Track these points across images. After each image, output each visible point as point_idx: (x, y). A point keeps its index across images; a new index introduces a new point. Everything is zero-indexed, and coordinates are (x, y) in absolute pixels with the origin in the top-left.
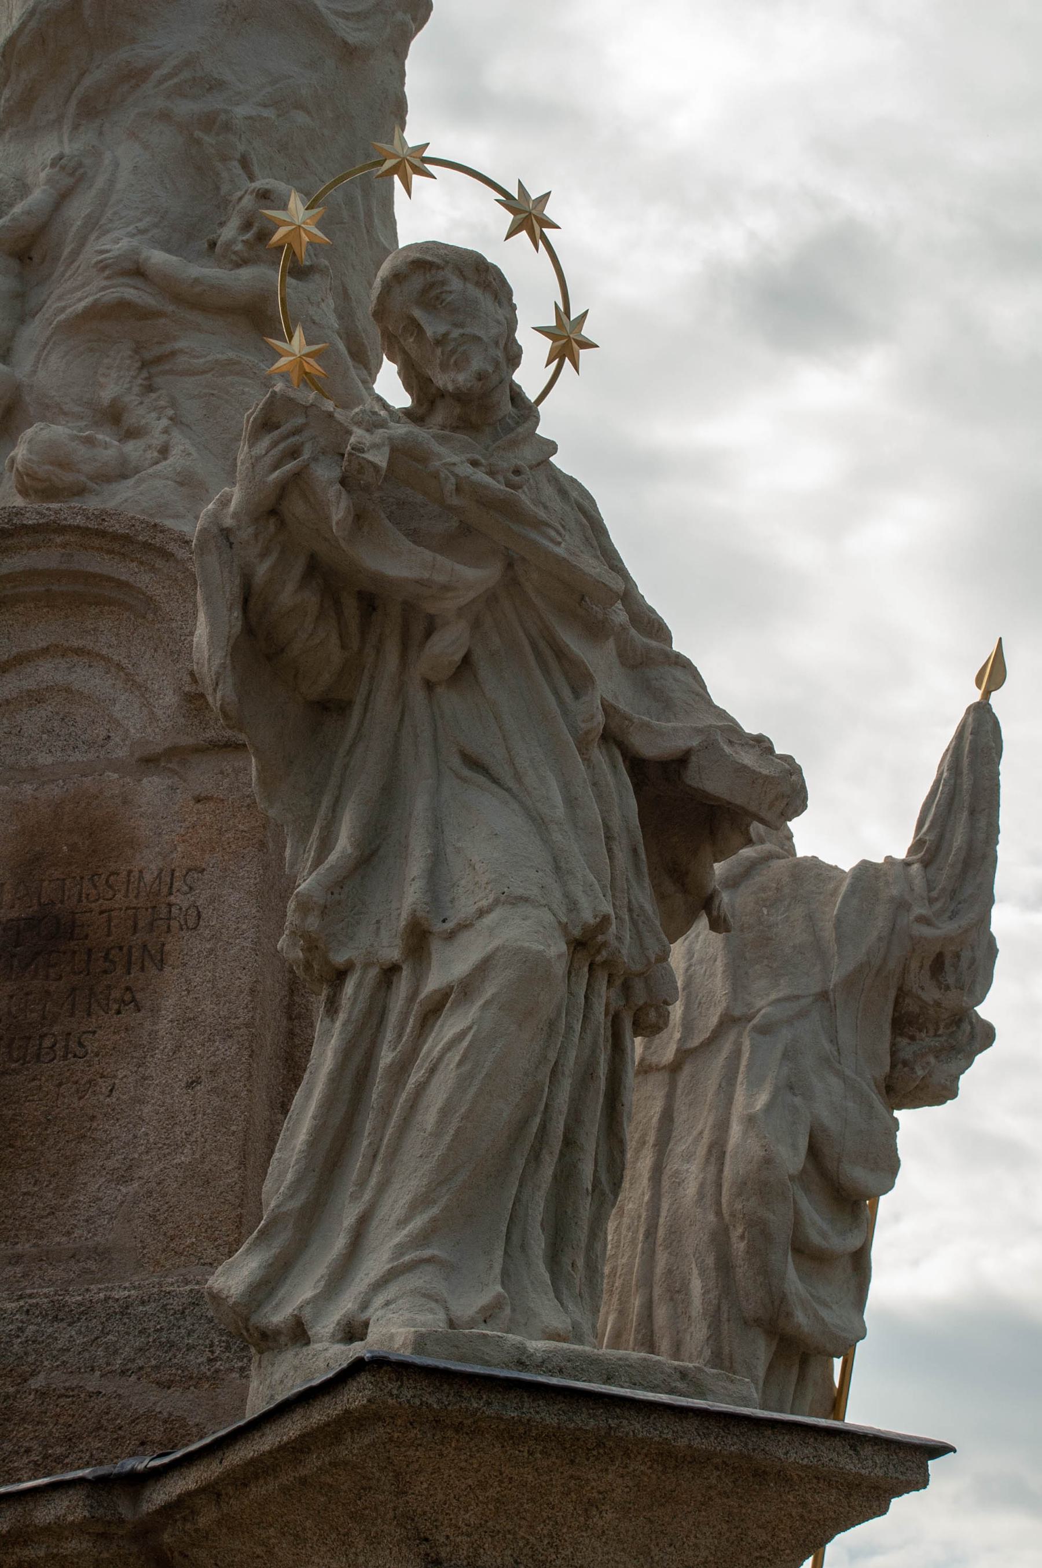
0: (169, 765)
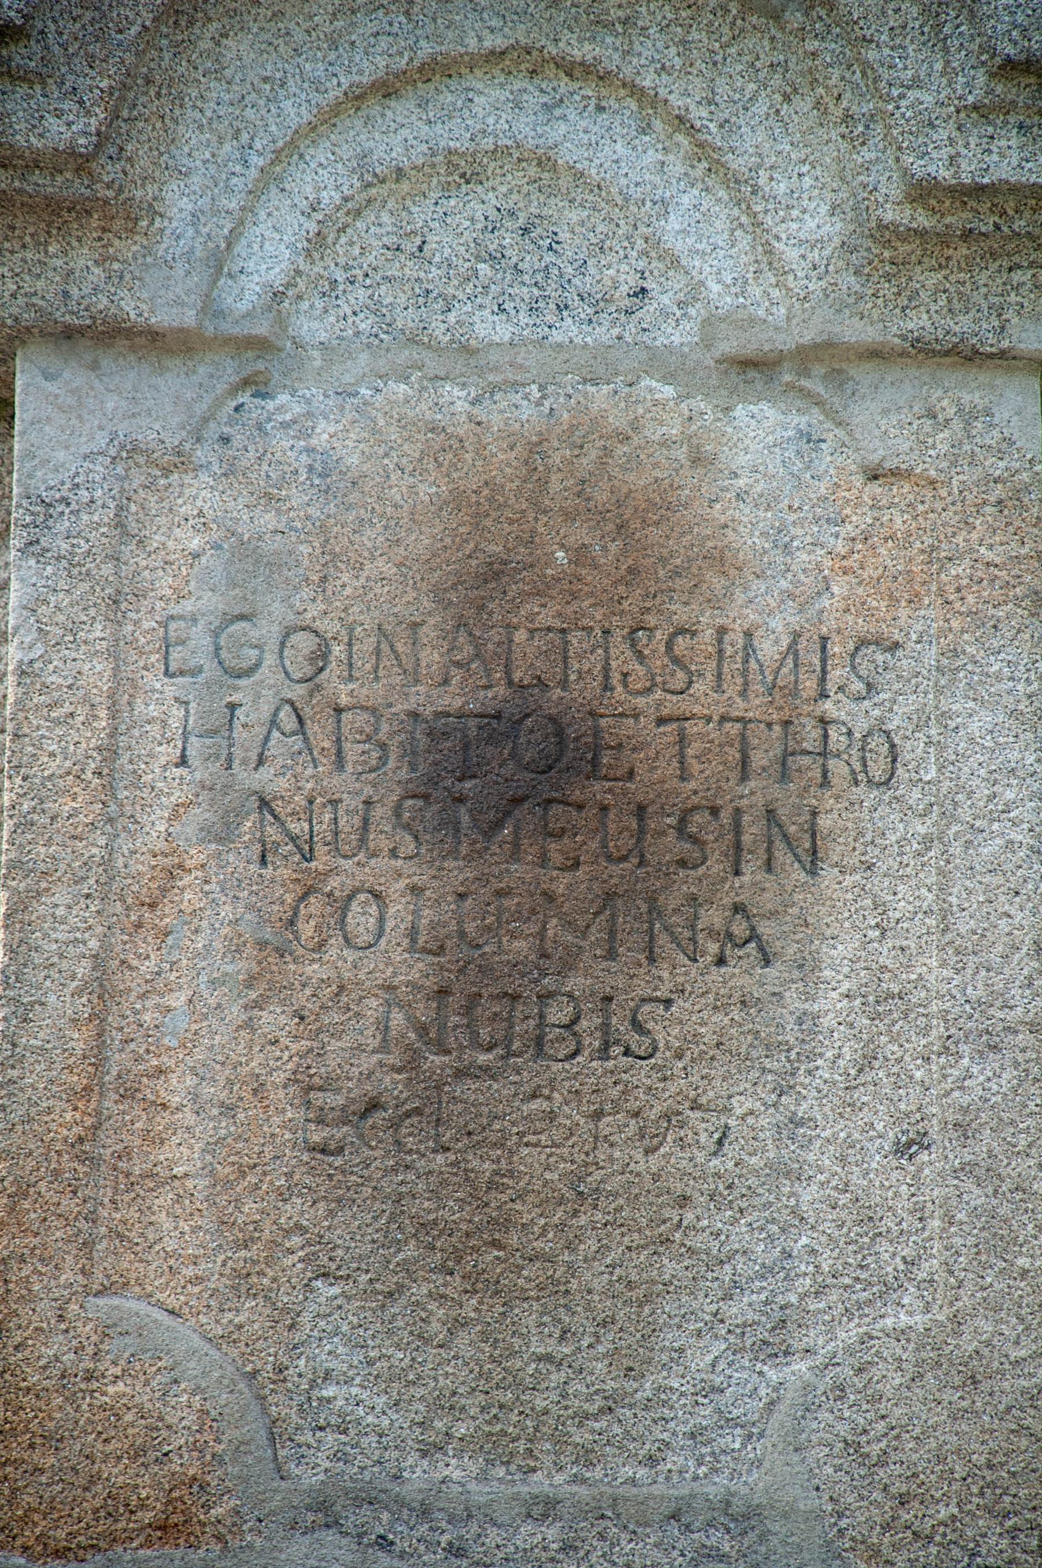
0: (804, 383)
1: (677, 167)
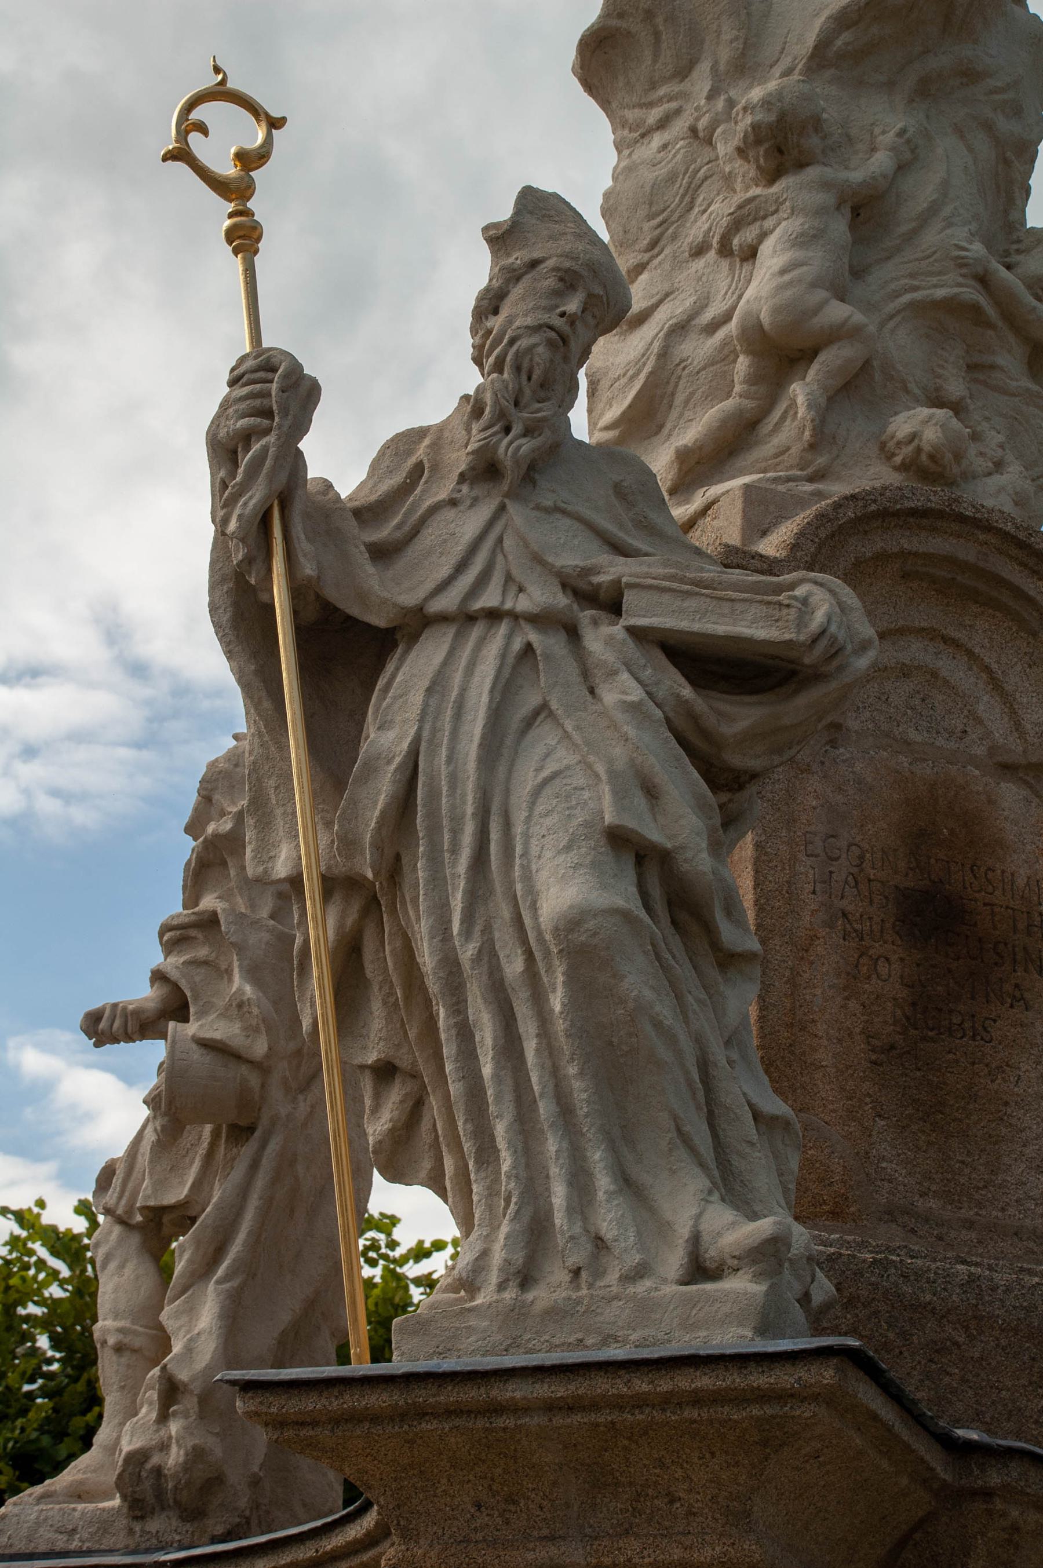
1: (981, 686)
